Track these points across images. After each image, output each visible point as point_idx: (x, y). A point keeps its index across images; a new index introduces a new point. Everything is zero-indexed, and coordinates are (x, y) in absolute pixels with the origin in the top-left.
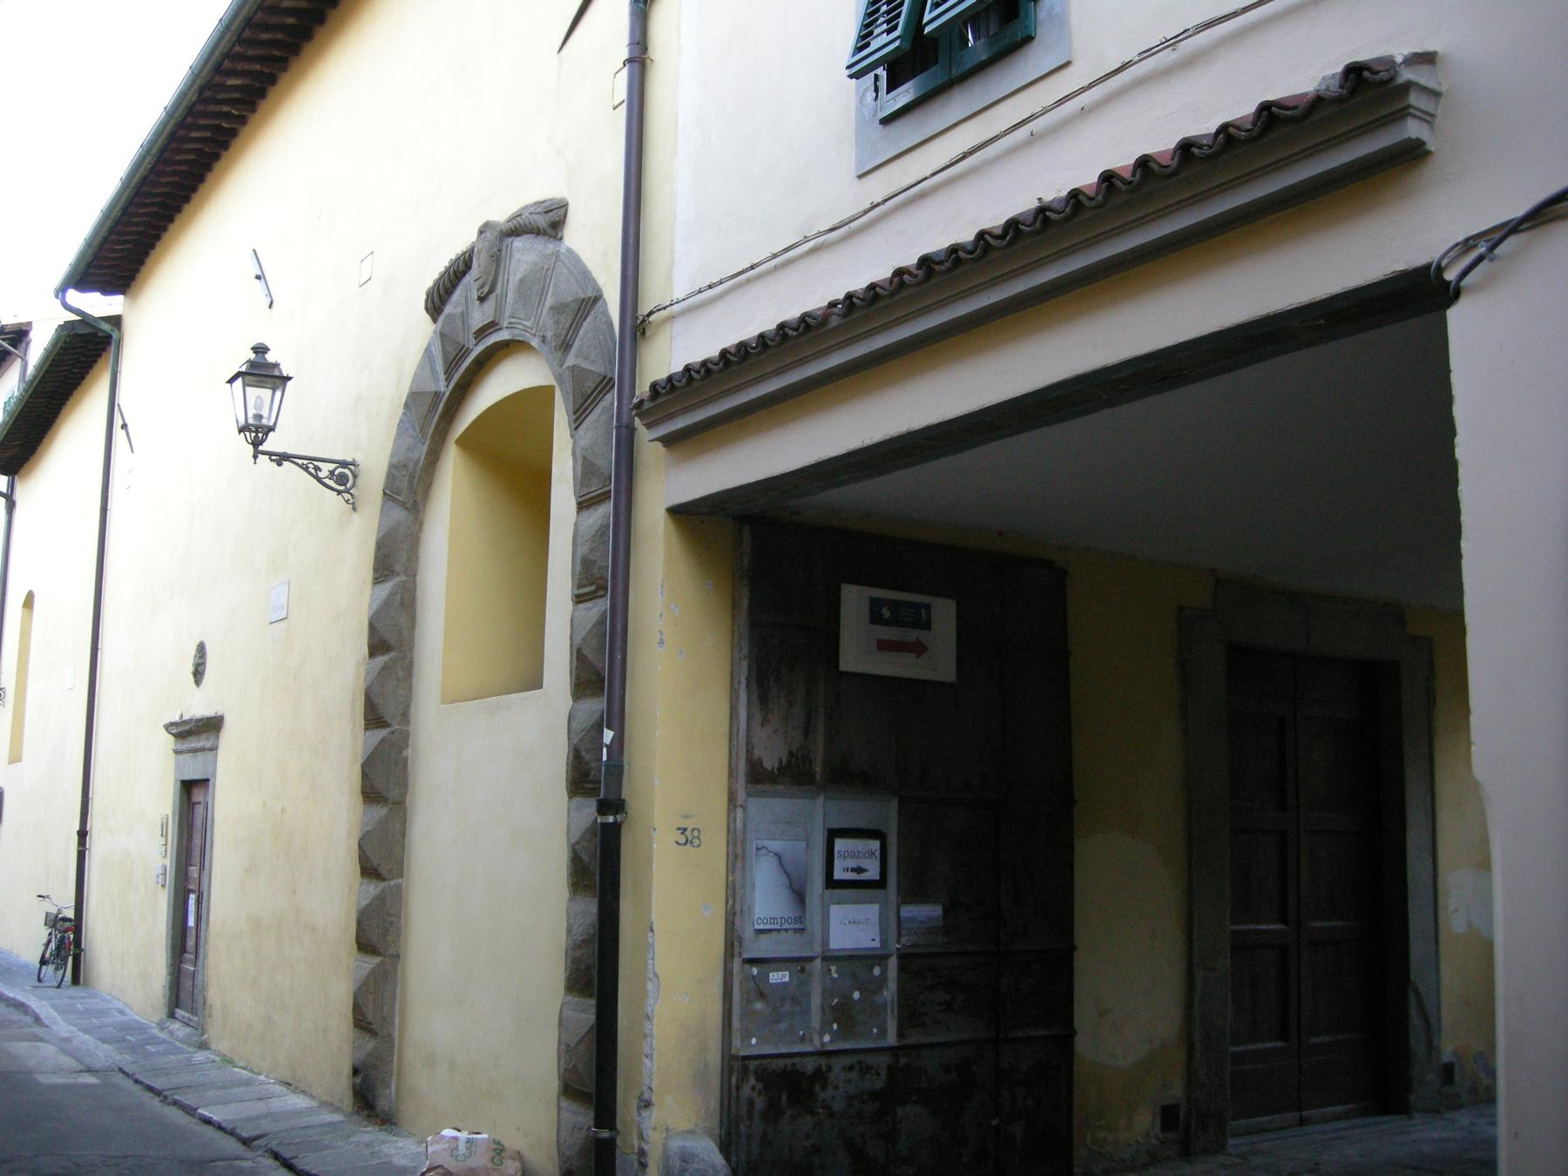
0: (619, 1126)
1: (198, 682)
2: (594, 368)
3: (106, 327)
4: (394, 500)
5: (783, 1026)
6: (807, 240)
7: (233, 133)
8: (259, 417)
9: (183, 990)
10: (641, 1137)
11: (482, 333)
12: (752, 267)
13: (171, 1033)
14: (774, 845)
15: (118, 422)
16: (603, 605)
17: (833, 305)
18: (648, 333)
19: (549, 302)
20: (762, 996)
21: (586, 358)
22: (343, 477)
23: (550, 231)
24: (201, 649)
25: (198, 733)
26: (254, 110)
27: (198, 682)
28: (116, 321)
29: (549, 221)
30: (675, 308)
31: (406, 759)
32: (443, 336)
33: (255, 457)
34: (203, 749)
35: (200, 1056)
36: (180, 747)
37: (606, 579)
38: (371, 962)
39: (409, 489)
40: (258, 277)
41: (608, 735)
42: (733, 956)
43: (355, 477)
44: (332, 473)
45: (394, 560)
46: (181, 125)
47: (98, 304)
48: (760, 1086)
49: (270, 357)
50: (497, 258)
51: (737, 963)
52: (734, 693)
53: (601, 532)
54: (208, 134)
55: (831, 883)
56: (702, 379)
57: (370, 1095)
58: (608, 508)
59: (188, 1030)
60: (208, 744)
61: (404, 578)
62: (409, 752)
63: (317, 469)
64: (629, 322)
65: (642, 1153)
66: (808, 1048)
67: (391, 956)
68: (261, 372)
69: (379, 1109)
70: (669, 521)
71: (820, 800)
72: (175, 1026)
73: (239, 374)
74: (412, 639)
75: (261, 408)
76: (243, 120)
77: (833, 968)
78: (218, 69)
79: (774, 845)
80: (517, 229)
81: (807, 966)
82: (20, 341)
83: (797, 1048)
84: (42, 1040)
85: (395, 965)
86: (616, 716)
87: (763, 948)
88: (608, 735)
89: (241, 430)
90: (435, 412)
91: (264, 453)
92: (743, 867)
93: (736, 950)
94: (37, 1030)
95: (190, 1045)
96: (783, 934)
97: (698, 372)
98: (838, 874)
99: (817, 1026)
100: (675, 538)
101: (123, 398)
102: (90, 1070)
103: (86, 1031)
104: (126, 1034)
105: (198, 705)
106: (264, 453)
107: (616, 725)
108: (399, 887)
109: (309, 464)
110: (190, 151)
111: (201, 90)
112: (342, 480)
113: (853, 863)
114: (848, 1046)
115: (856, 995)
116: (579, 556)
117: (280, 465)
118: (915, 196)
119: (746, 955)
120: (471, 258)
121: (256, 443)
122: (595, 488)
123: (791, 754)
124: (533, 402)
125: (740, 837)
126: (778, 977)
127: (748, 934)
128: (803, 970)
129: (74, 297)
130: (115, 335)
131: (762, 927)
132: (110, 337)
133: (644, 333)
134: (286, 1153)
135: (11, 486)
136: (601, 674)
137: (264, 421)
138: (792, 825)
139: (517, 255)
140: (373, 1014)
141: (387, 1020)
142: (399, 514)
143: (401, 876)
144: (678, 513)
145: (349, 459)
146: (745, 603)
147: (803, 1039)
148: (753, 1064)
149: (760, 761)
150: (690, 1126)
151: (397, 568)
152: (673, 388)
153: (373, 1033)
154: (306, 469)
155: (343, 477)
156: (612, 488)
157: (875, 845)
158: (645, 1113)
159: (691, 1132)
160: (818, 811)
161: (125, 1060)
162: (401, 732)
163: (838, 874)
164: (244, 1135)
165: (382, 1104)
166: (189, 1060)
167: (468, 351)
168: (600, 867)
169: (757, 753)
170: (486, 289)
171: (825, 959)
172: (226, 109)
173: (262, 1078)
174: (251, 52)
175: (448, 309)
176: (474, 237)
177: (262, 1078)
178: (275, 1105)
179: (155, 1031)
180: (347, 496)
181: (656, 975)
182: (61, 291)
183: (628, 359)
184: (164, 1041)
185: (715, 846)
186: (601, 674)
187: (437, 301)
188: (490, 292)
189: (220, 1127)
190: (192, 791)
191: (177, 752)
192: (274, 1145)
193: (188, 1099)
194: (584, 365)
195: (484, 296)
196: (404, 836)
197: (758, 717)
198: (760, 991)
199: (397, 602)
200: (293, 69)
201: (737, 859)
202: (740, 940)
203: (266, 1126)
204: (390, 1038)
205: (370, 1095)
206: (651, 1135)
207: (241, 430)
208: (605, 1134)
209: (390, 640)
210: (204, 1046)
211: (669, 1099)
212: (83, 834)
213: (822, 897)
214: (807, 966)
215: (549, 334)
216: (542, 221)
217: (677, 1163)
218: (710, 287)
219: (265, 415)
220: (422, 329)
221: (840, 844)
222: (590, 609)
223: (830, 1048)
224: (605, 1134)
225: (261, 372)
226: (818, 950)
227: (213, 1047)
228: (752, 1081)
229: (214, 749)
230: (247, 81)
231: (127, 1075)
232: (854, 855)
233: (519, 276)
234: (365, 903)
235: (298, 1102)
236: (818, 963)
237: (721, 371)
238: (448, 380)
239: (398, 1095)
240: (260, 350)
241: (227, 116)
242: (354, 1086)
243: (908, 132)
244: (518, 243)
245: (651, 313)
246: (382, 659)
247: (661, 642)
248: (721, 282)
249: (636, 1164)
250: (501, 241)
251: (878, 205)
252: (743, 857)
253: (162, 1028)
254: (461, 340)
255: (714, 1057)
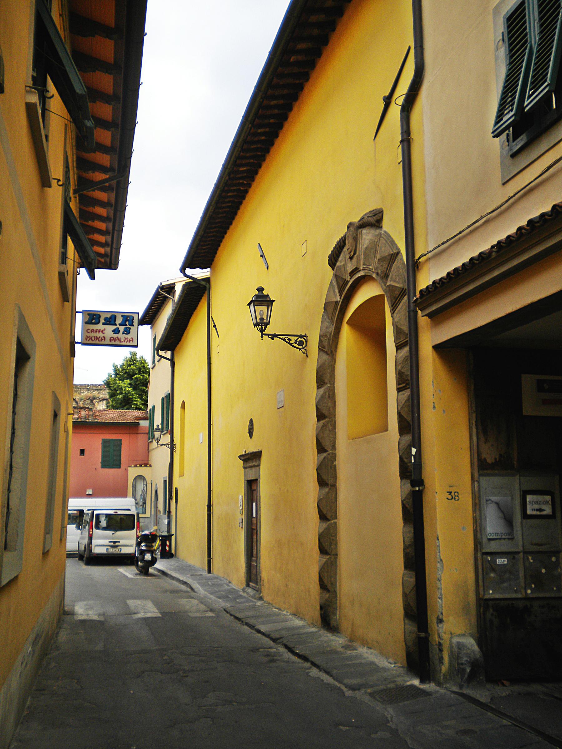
0: (430, 631)
1: (251, 437)
2: (398, 285)
3: (203, 283)
4: (323, 351)
5: (505, 585)
6: (482, 217)
7: (246, 192)
8: (262, 319)
9: (252, 575)
10: (439, 636)
11: (352, 273)
12: (460, 233)
13: (248, 593)
14: (494, 499)
15: (212, 324)
16: (407, 393)
17: (493, 247)
18: (419, 268)
19: (378, 256)
20: (493, 570)
21: (395, 281)
22: (301, 342)
23: (376, 224)
24: (251, 421)
25: (251, 459)
26: (253, 180)
27: (251, 437)
28: (207, 280)
29: (374, 220)
30: (430, 255)
31: (335, 466)
32: (336, 276)
33: (262, 337)
34: (254, 466)
35: (259, 603)
36: (245, 466)
37: (409, 381)
38: (325, 558)
39: (329, 346)
40: (261, 256)
41: (414, 451)
42: (477, 551)
43: (306, 342)
44: (296, 341)
45: (325, 378)
46: (223, 191)
47: (199, 273)
48: (495, 613)
49: (265, 292)
50: (356, 239)
51: (479, 555)
52: (470, 428)
53: (405, 360)
54: (235, 193)
55: (525, 516)
56: (441, 287)
57: (327, 619)
58: (407, 349)
59: (255, 592)
60: (256, 464)
61: (329, 385)
62: (336, 463)
63: (289, 339)
64: (410, 262)
65: (440, 644)
66: (519, 596)
67: (334, 555)
68: (261, 299)
69: (332, 625)
70: (435, 353)
71: (518, 477)
72: (250, 590)
73: (252, 302)
74: (335, 412)
75: (263, 315)
76: (250, 186)
77: (530, 558)
78: (235, 164)
79: (494, 499)
80: (363, 224)
81: (516, 556)
82: (171, 292)
83: (514, 596)
84: (193, 598)
85: (336, 559)
86: (417, 442)
87: (493, 547)
88: (414, 451)
89: (255, 325)
90: (335, 312)
91: (266, 335)
92: (480, 510)
93: (479, 548)
94: (193, 594)
95: (255, 599)
96: (503, 541)
97: (438, 284)
98: (529, 512)
99: (523, 585)
100: (437, 360)
101: (213, 314)
102: (211, 610)
103: (212, 594)
104: (230, 594)
105: (252, 449)
106: (266, 335)
107: (417, 446)
108: (335, 523)
109: (286, 338)
110: (229, 202)
111: (229, 174)
112: (301, 343)
113: (536, 506)
114: (541, 595)
115: (544, 571)
116: (398, 370)
117: (273, 339)
118: (528, 191)
119: (484, 551)
120: (345, 239)
121: (262, 331)
122: (402, 340)
123: (501, 455)
124: (374, 303)
125: (477, 495)
126: (500, 561)
127: (485, 541)
128: (514, 558)
129: (188, 271)
130: (207, 286)
131: (491, 537)
132: (206, 287)
133: (418, 267)
134: (291, 645)
135: (172, 355)
136: (410, 424)
137: (265, 321)
138: (502, 489)
139: (364, 236)
140: (327, 583)
141: (334, 584)
142: (325, 357)
143: (336, 518)
144: (436, 348)
145: (304, 334)
146: (472, 388)
147: (516, 592)
148: (491, 603)
149: (485, 459)
150: (462, 632)
151: (326, 381)
152: (429, 292)
153: (328, 591)
154: (285, 340)
155: (301, 342)
156: (409, 340)
157: (548, 498)
158: (440, 626)
159: (463, 635)
160: (516, 483)
161: (227, 605)
162: (333, 453)
163: (529, 512)
164: (274, 637)
165: (333, 623)
166: (254, 605)
167: (348, 282)
168: (414, 512)
169: (484, 456)
170: (352, 253)
171: (525, 553)
172: (241, 181)
173: (284, 612)
174: (248, 155)
175: (338, 264)
176: (346, 230)
177: (284, 612)
178: (288, 624)
179: (242, 593)
180: (303, 350)
181: (441, 560)
182: (183, 270)
183: (411, 279)
184: (244, 597)
185: (467, 500)
186: (410, 424)
187: (333, 260)
188: (355, 254)
189: (263, 634)
190: (252, 485)
191: (244, 468)
192: (285, 641)
193: (252, 621)
194: (394, 284)
195: (352, 256)
196: (336, 500)
197: (482, 439)
198: (493, 568)
199: (327, 396)
200: (267, 160)
201: (477, 506)
202: (481, 543)
203: (284, 633)
204: (335, 591)
205: (327, 619)
206: (446, 637)
207: (255, 325)
208: (423, 635)
209: (325, 414)
210: (261, 599)
211: (451, 618)
212: (209, 506)
213: (522, 523)
214: (516, 556)
215: (379, 271)
216: (372, 220)
217: (456, 650)
218: (443, 244)
219: (265, 318)
220: (330, 273)
221: (529, 498)
222: (404, 394)
223: (531, 596)
224: (423, 635)
225: (261, 299)
226: (520, 549)
227: (265, 599)
228: (491, 611)
229: (259, 466)
230: (248, 168)
231: (227, 612)
232: (537, 503)
233: (365, 246)
234: (321, 531)
235: (298, 622)
236: (521, 554)
237: (448, 282)
238: (341, 296)
239: (340, 619)
240: (260, 290)
241: (242, 185)
242: (321, 615)
243: (523, 160)
244: (364, 231)
245: (420, 258)
246: (322, 422)
247: (434, 407)
248: (447, 241)
249: (437, 649)
250: (357, 231)
251: (512, 197)
252: (480, 505)
253: (244, 591)
254: (344, 277)
255: (472, 598)
